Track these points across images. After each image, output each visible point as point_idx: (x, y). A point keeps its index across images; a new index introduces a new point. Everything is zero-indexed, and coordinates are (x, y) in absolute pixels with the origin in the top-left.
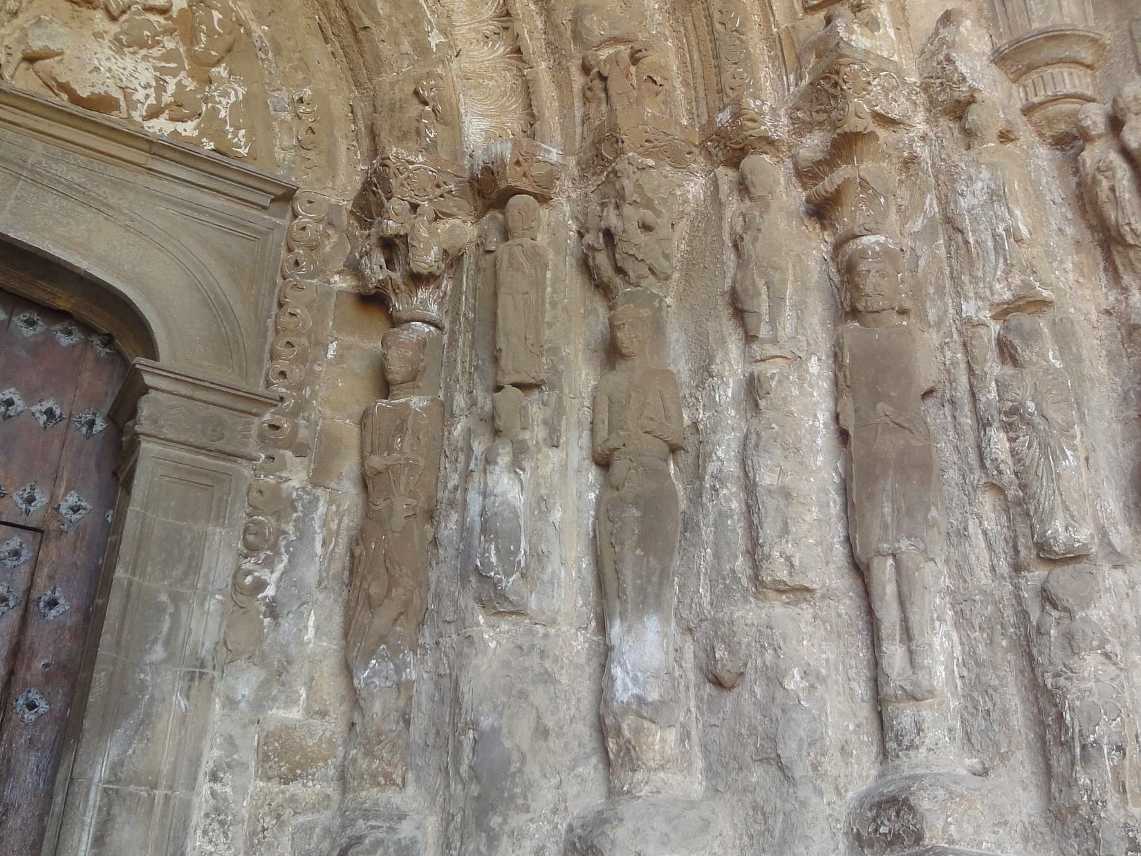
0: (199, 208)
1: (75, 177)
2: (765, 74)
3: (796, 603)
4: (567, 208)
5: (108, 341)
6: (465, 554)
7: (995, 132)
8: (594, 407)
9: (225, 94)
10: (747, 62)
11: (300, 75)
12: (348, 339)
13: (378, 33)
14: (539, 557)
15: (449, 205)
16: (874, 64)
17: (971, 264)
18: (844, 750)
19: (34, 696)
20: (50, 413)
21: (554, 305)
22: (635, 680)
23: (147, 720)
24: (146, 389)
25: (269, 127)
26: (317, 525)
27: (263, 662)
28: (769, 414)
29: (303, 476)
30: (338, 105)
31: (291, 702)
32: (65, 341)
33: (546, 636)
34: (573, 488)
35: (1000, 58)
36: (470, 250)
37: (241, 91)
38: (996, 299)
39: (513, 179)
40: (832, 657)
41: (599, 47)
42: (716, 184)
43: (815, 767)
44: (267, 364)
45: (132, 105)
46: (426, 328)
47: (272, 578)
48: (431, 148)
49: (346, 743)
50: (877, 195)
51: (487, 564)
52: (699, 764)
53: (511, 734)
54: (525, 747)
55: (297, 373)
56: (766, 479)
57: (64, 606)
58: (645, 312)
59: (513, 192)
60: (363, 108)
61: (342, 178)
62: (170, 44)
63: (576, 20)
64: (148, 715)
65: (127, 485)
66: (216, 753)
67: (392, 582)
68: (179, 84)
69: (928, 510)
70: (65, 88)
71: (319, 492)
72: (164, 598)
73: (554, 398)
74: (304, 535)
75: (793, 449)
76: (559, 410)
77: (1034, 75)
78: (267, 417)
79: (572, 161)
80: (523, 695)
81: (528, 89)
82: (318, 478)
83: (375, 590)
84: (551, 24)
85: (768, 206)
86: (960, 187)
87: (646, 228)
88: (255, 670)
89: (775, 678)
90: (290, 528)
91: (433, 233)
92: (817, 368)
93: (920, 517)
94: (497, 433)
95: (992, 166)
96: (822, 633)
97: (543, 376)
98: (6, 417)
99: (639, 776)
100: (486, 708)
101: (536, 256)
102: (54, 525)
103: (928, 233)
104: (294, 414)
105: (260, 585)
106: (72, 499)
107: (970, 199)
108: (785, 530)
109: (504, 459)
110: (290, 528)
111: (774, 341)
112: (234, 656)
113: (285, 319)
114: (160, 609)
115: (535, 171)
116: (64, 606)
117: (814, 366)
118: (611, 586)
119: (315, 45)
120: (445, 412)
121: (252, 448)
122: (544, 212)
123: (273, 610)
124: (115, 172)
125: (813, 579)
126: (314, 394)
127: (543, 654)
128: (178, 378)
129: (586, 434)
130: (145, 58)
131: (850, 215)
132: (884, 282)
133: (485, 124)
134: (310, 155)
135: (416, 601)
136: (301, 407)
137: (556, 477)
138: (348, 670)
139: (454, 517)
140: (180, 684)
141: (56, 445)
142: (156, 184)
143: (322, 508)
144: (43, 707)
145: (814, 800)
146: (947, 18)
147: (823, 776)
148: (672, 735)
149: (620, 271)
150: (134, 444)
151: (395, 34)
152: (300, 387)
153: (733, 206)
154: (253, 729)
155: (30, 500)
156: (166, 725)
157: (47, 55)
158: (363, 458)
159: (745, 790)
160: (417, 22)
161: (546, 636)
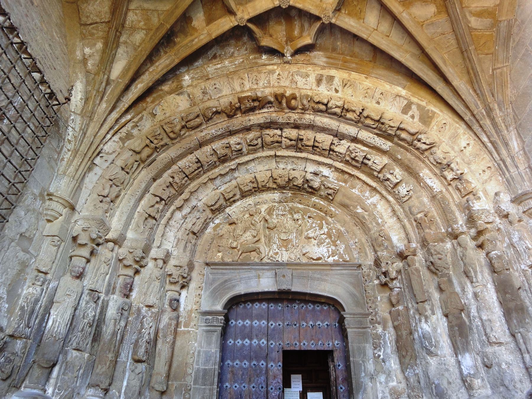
0: (343, 274)
1: (319, 276)
2: (457, 214)
3: (500, 346)
4: (421, 256)
5: (333, 306)
6: (421, 343)
7: (516, 221)
8: (440, 302)
9: (341, 248)
10: (452, 212)
11: (354, 237)
12: (382, 295)
13: (368, 223)
14: (437, 342)
15: (395, 260)
16: (481, 212)
17: (520, 256)
18: (521, 381)
19: (341, 386)
20: (327, 325)
21: (424, 280)
22: (467, 369)
23: (365, 389)
24: (345, 318)
25: (351, 251)
26: (387, 339)
27: (384, 373)
28: (481, 301)
29: (381, 329)
30: (364, 240)
31: (393, 381)
32: (325, 308)
33: (444, 360)
34: (441, 323)
35: (513, 201)
36: (402, 269)
37: (344, 246)
38: (528, 264)
39: (406, 254)
40: (512, 359)
41: (417, 214)
42: (453, 244)
43: (514, 386)
44: (366, 305)
45: (324, 257)
46: (398, 289)
47: (381, 354)
48: (386, 248)
49: (407, 389)
50: (492, 241)
51: (426, 345)
52: (489, 386)
53: (443, 385)
54: (447, 387)
55: (373, 306)
56: (484, 318)
57: (341, 366)
58: (445, 279)
59: (407, 256)
60: (369, 240)
61: (369, 257)
62: (327, 241)
63: (410, 210)
64: (365, 388)
65: (346, 337)
66: (381, 395)
67: (407, 352)
68: (332, 249)
69: (525, 320)
70: (312, 258)
71: (385, 332)
72: (361, 362)
73: (431, 304)
74: (385, 343)
75: (489, 309)
76: (433, 305)
77: (523, 203)
78: (370, 317)
79: (419, 245)
80: (443, 375)
81: (404, 227)
82: (384, 329)
83: (404, 353)
84: (405, 211)
85: (466, 249)
86: (512, 236)
87: (440, 259)
88: (384, 375)
89: (499, 365)
90: (382, 342)
91: (393, 268)
92: (490, 287)
93: (524, 322)
94: (420, 314)
95: (518, 231)
96: (508, 353)
97: (427, 298)
98: (319, 328)
99: (474, 391)
100: (435, 379)
101: (417, 270)
102: (335, 348)
103: (508, 247)
104: (375, 315)
105: (379, 356)
106: (336, 342)
107: (515, 239)
108: (492, 330)
109: (423, 320)
110: (382, 342)
111: (478, 282)
112: (378, 372)
113: (367, 294)
114: (361, 364)
115: (411, 250)
116: (341, 366)
117: (489, 286)
118: (456, 347)
119: (355, 228)
120: (407, 309)
121: (369, 325)
122: (416, 258)
123: (384, 361)
124: (325, 272)
125: (502, 340)
126: (378, 310)
127: (445, 364)
128: (350, 314)
129: (440, 309)
130: (324, 246)
131: (488, 246)
132: (499, 264)
133: (397, 237)
134: (361, 254)
135: (413, 354)
136: (376, 313)
137: (436, 322)
138: (403, 372)
139: (416, 333)
140: (369, 380)
141: (330, 331)
142: (333, 272)
143: (387, 335)
144: (344, 388)
145: (516, 394)
146: (496, 194)
147: (517, 388)
148: (479, 381)
149: (437, 269)
150: (346, 330)
151: (371, 222)
152: (375, 309)
153: (459, 249)
154: (387, 388)
155: (329, 344)
156: (369, 390)
157: (307, 253)
158: (393, 323)
159: (500, 393)
160: (375, 218)
161: (444, 360)
